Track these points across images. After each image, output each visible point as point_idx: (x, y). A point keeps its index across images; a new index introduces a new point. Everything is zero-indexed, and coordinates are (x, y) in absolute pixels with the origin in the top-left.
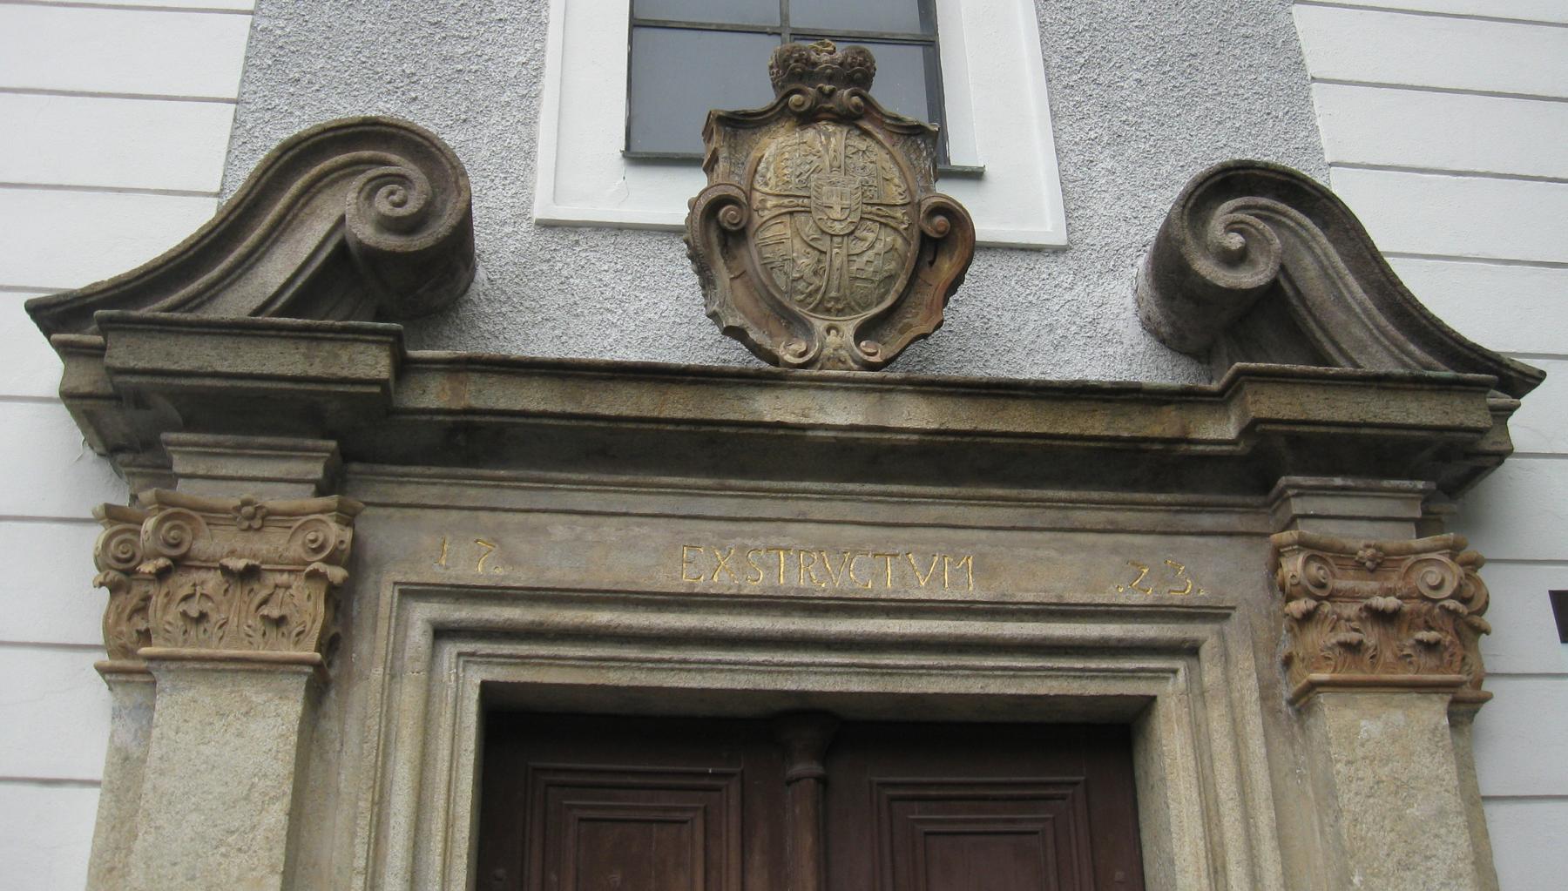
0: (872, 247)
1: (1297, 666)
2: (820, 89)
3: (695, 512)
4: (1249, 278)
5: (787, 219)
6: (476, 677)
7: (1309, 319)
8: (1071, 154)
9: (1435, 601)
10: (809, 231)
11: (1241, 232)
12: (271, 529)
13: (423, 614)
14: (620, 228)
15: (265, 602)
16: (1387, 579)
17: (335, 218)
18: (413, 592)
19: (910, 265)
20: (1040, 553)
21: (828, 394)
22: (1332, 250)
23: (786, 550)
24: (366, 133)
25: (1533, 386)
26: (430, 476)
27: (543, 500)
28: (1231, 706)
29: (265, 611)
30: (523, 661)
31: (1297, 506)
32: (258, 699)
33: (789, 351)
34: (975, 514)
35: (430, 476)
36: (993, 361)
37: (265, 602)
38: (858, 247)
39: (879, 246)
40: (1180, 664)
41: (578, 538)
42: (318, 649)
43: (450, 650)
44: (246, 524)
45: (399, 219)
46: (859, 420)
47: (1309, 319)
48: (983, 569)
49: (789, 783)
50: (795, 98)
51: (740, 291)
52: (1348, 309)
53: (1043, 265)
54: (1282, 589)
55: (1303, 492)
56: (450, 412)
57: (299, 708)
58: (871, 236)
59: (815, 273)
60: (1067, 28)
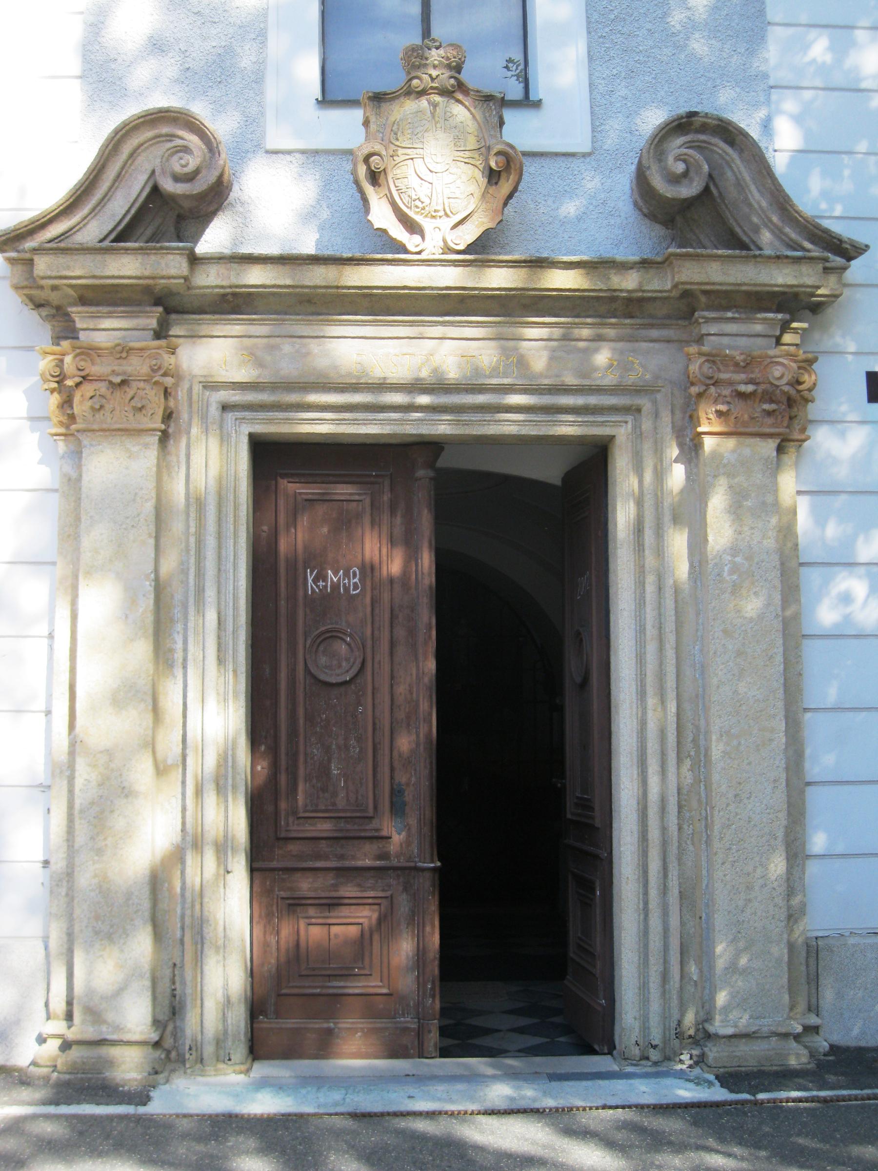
2: (430, 76)
4: (687, 191)
6: (246, 429)
7: (727, 212)
8: (600, 86)
9: (777, 386)
11: (684, 161)
12: (133, 357)
15: (132, 398)
16: (752, 372)
17: (149, 172)
22: (743, 169)
24: (163, 117)
25: (861, 254)
26: (214, 320)
28: (656, 442)
29: (133, 403)
32: (135, 449)
35: (214, 320)
36: (540, 230)
37: (132, 398)
40: (629, 418)
41: (297, 351)
42: (163, 422)
43: (230, 416)
44: (118, 356)
47: (727, 212)
49: (416, 480)
50: (415, 82)
55: (708, 320)
56: (222, 287)
57: (156, 453)
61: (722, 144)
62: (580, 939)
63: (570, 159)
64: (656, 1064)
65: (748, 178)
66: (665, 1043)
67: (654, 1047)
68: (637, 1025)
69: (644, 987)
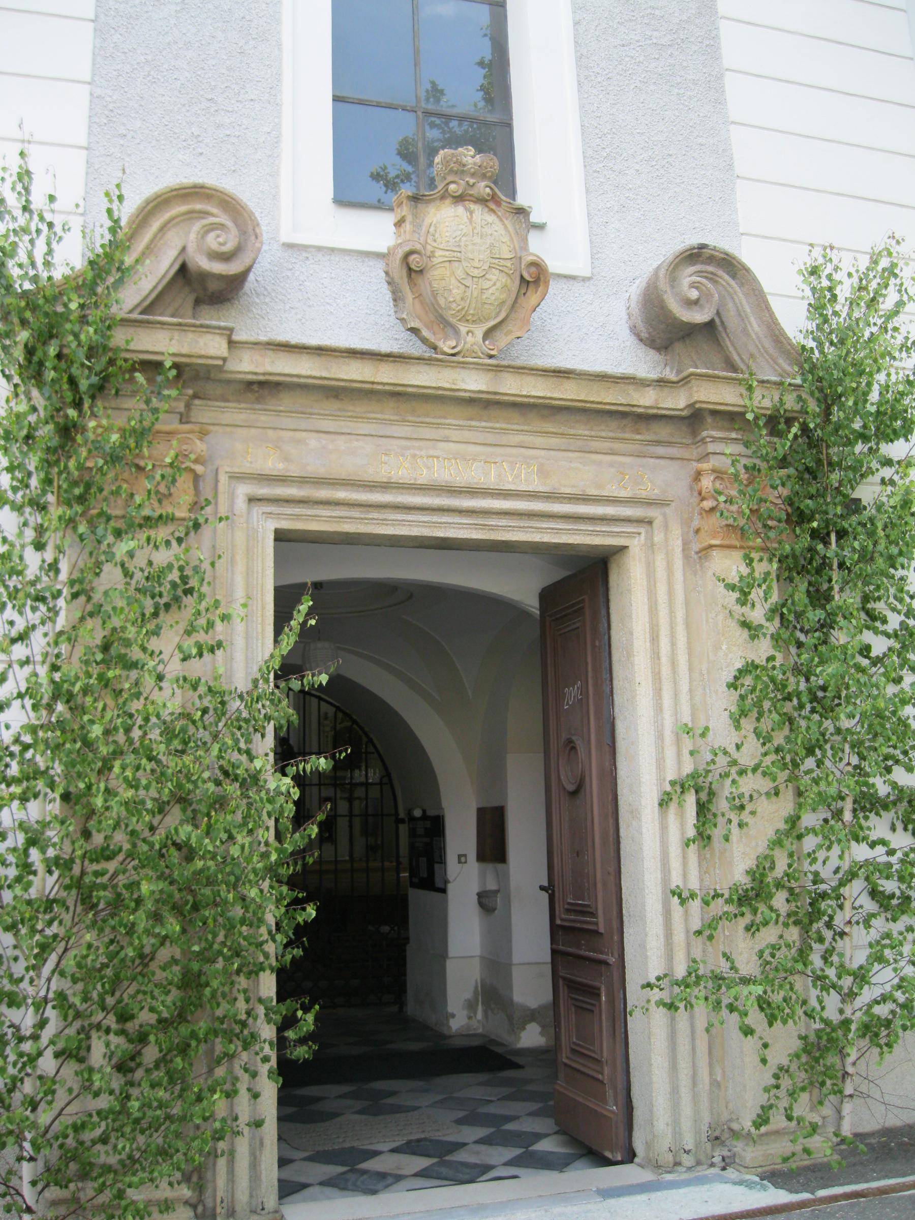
0: (494, 284)
1: (702, 534)
3: (388, 434)
4: (699, 317)
5: (447, 264)
6: (271, 526)
10: (460, 273)
11: (697, 288)
13: (243, 490)
14: (333, 250)
17: (179, 248)
18: (238, 477)
19: (513, 297)
20: (573, 465)
21: (467, 372)
22: (744, 302)
23: (438, 457)
27: (304, 425)
28: (667, 554)
30: (298, 517)
31: (711, 448)
33: (446, 346)
34: (539, 441)
36: (547, 347)
38: (487, 284)
39: (499, 285)
45: (223, 253)
46: (483, 388)
48: (543, 473)
50: (452, 187)
51: (418, 305)
52: (749, 335)
53: (577, 287)
54: (700, 494)
55: (715, 439)
56: (256, 374)
58: (494, 278)
59: (462, 299)
60: (597, 131)
61: (726, 277)
62: (575, 1043)
63: (571, 282)
64: (690, 1169)
65: (748, 310)
66: (696, 1147)
67: (687, 1152)
68: (669, 1131)
69: (675, 1090)
